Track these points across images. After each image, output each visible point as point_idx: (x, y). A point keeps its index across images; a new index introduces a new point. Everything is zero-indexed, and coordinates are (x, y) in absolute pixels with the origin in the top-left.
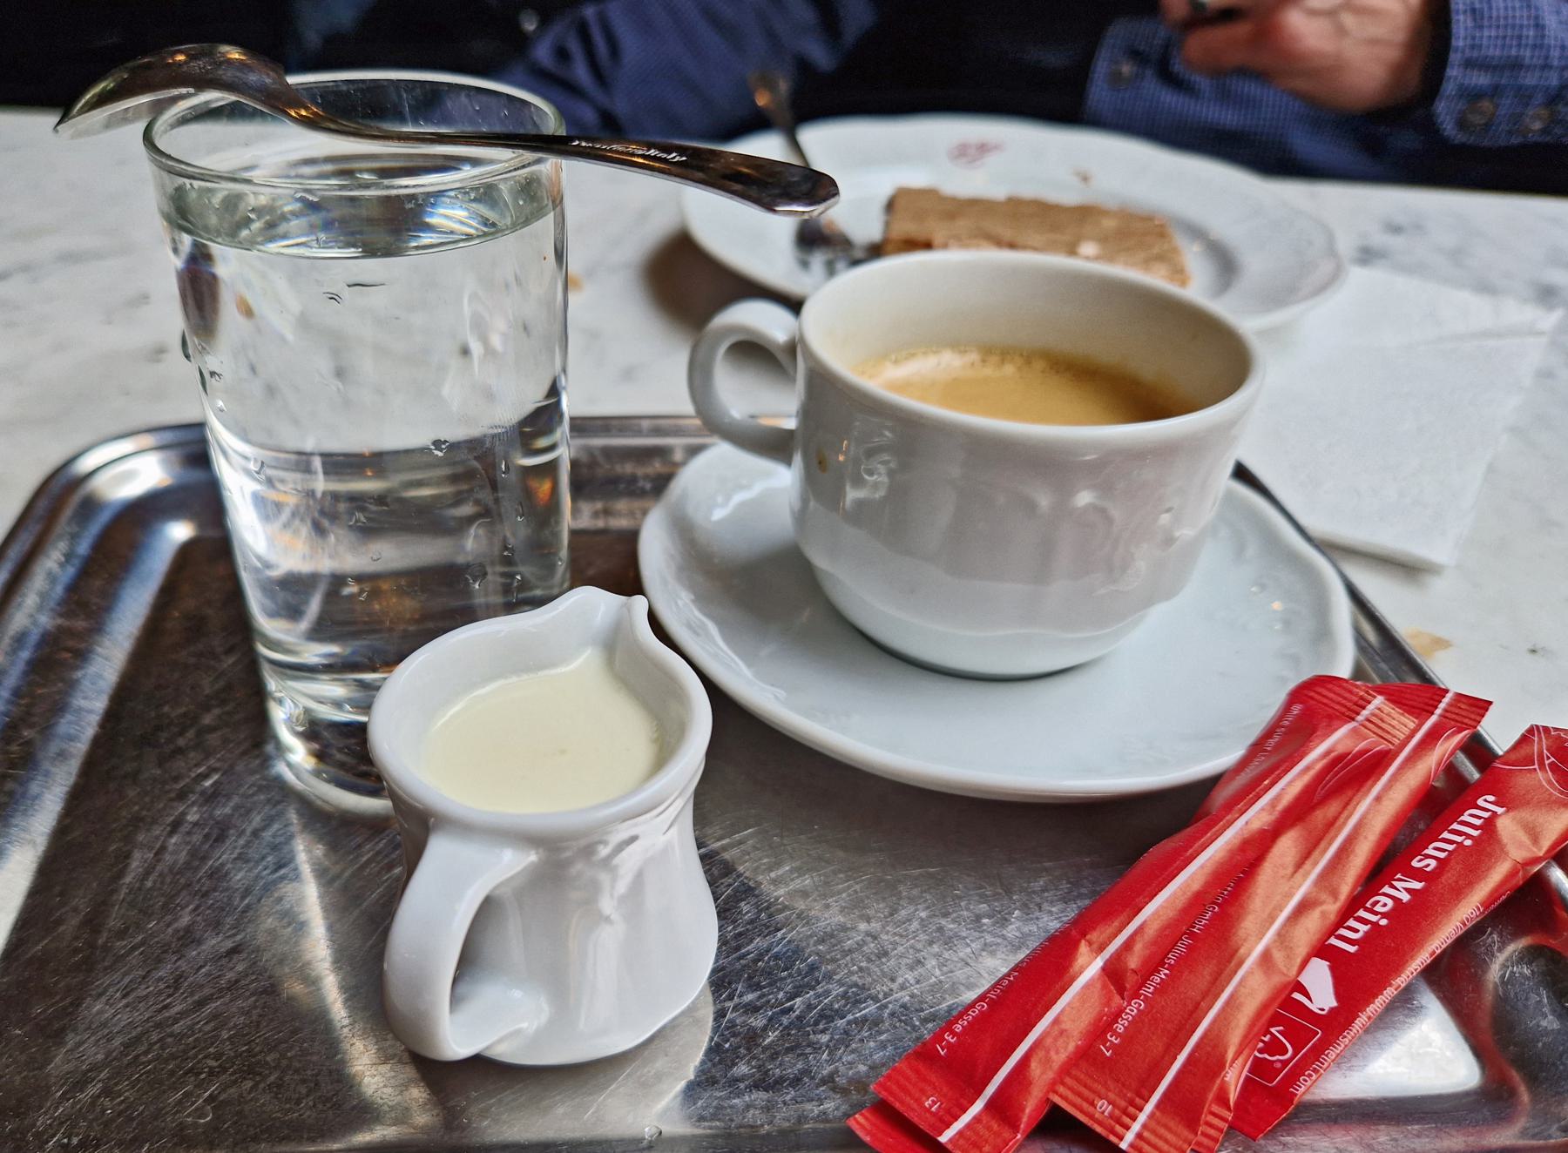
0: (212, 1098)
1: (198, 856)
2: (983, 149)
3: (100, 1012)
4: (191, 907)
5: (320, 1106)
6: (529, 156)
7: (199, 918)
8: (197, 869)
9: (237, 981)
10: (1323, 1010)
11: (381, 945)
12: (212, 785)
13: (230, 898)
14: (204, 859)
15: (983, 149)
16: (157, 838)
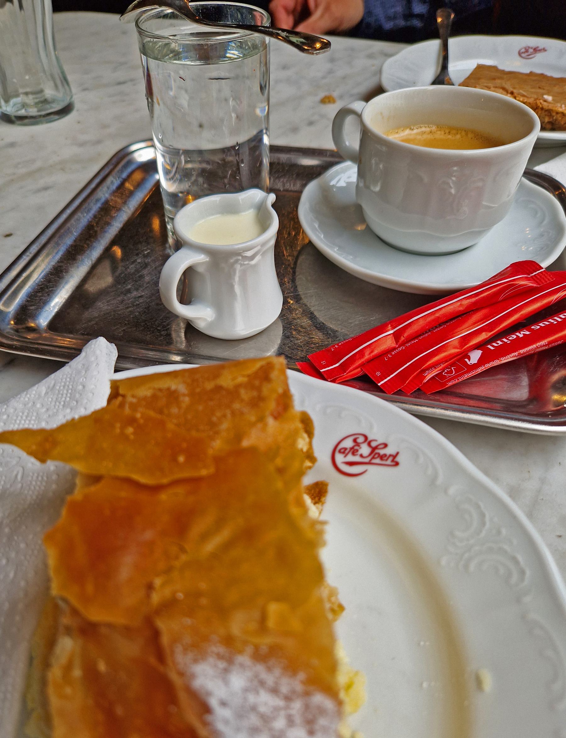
0: (124, 330)
1: (137, 271)
2: (536, 50)
3: (99, 305)
4: (132, 284)
5: (152, 338)
6: (248, 32)
7: (133, 287)
8: (136, 275)
9: (139, 304)
10: (471, 364)
11: (160, 268)
12: (147, 253)
13: (143, 284)
14: (139, 272)
15: (536, 50)
16: (127, 265)
